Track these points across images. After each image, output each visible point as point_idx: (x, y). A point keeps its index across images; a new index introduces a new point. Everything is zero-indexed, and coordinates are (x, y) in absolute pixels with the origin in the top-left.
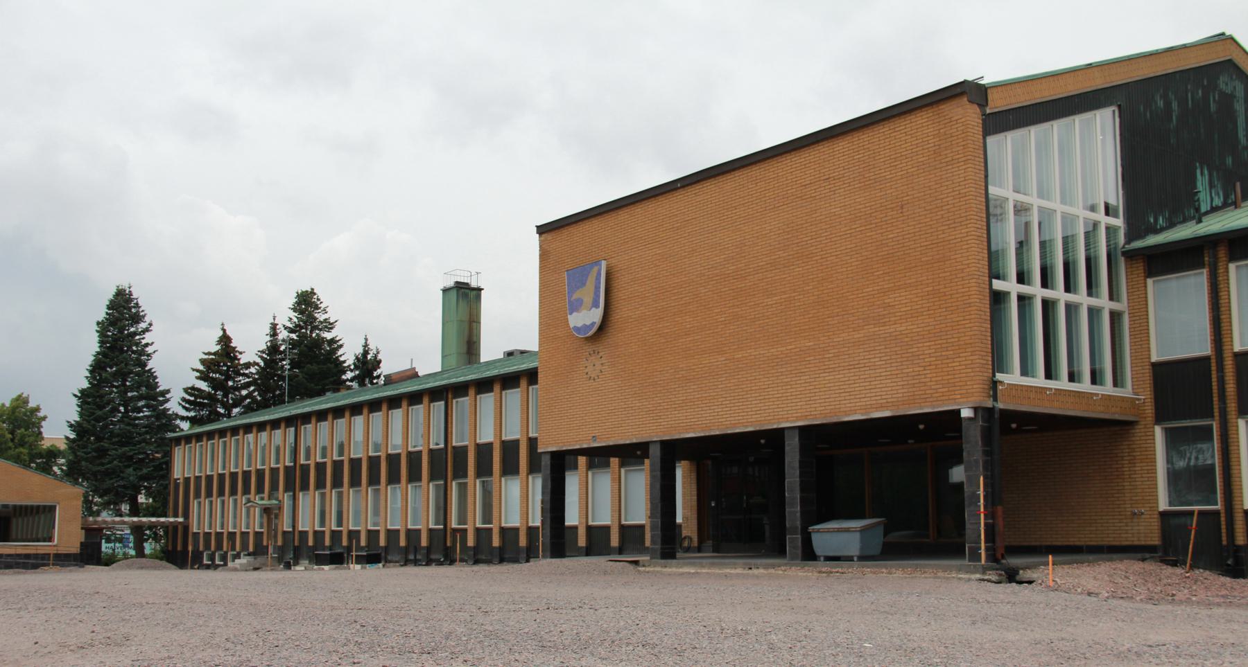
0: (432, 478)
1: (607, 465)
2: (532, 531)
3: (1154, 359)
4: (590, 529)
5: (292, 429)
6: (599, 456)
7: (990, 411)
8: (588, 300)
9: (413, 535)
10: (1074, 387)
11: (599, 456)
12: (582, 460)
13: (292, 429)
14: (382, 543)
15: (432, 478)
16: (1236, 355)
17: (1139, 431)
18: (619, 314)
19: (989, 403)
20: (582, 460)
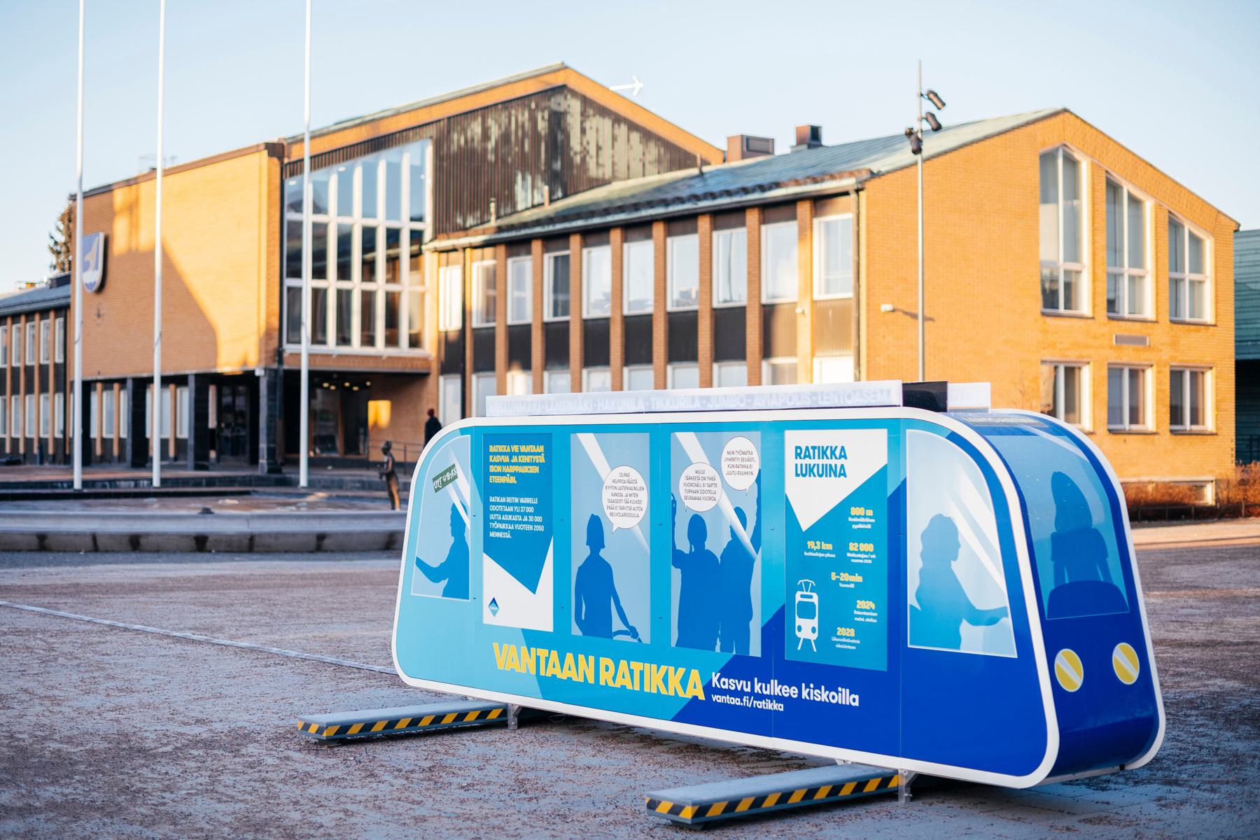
0: (57, 390)
1: (111, 388)
2: (121, 441)
3: (510, 322)
4: (177, 440)
5: (62, 320)
6: (108, 384)
7: (276, 371)
8: (92, 264)
9: (43, 443)
10: (368, 350)
11: (108, 384)
12: (99, 386)
13: (62, 320)
14: (22, 450)
15: (57, 390)
16: (474, 330)
17: (431, 380)
18: (110, 277)
19: (275, 366)
20: (99, 386)
